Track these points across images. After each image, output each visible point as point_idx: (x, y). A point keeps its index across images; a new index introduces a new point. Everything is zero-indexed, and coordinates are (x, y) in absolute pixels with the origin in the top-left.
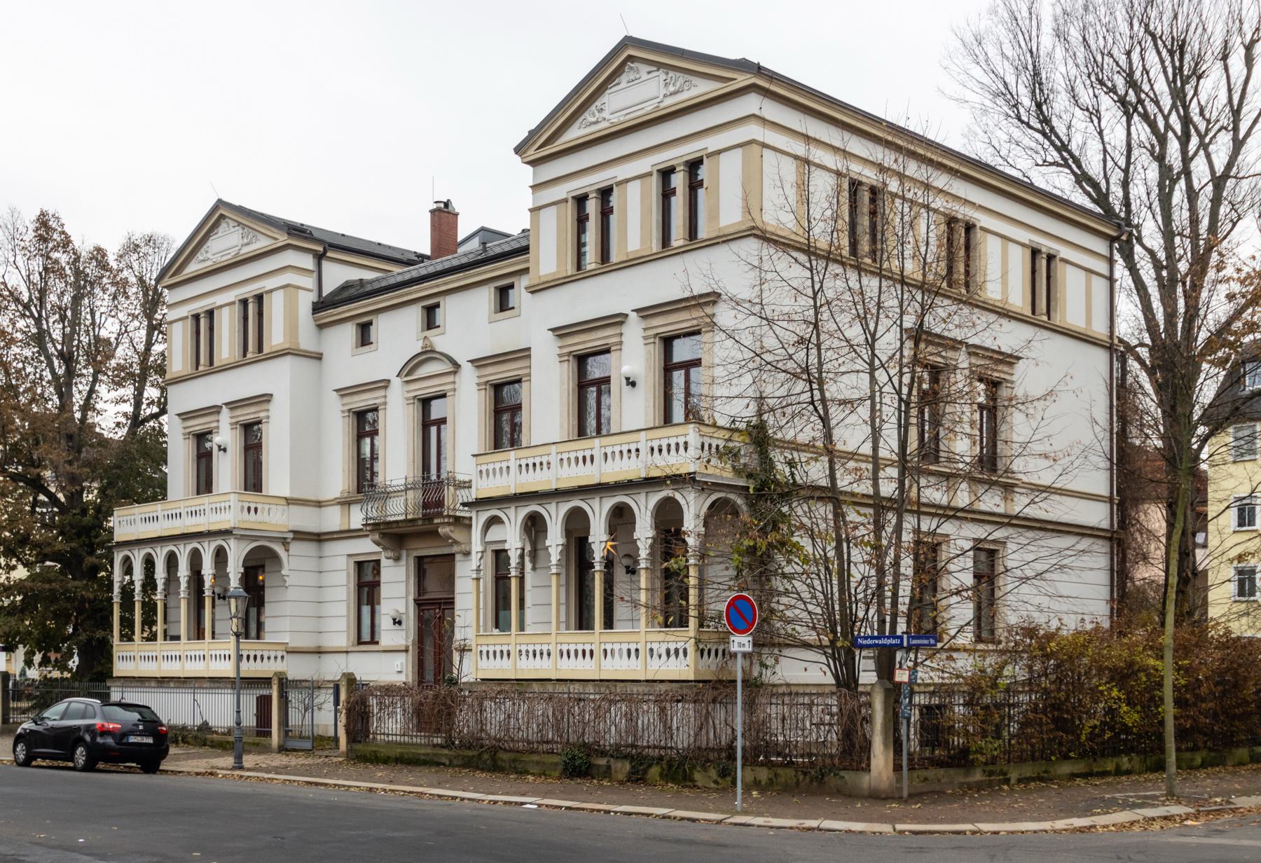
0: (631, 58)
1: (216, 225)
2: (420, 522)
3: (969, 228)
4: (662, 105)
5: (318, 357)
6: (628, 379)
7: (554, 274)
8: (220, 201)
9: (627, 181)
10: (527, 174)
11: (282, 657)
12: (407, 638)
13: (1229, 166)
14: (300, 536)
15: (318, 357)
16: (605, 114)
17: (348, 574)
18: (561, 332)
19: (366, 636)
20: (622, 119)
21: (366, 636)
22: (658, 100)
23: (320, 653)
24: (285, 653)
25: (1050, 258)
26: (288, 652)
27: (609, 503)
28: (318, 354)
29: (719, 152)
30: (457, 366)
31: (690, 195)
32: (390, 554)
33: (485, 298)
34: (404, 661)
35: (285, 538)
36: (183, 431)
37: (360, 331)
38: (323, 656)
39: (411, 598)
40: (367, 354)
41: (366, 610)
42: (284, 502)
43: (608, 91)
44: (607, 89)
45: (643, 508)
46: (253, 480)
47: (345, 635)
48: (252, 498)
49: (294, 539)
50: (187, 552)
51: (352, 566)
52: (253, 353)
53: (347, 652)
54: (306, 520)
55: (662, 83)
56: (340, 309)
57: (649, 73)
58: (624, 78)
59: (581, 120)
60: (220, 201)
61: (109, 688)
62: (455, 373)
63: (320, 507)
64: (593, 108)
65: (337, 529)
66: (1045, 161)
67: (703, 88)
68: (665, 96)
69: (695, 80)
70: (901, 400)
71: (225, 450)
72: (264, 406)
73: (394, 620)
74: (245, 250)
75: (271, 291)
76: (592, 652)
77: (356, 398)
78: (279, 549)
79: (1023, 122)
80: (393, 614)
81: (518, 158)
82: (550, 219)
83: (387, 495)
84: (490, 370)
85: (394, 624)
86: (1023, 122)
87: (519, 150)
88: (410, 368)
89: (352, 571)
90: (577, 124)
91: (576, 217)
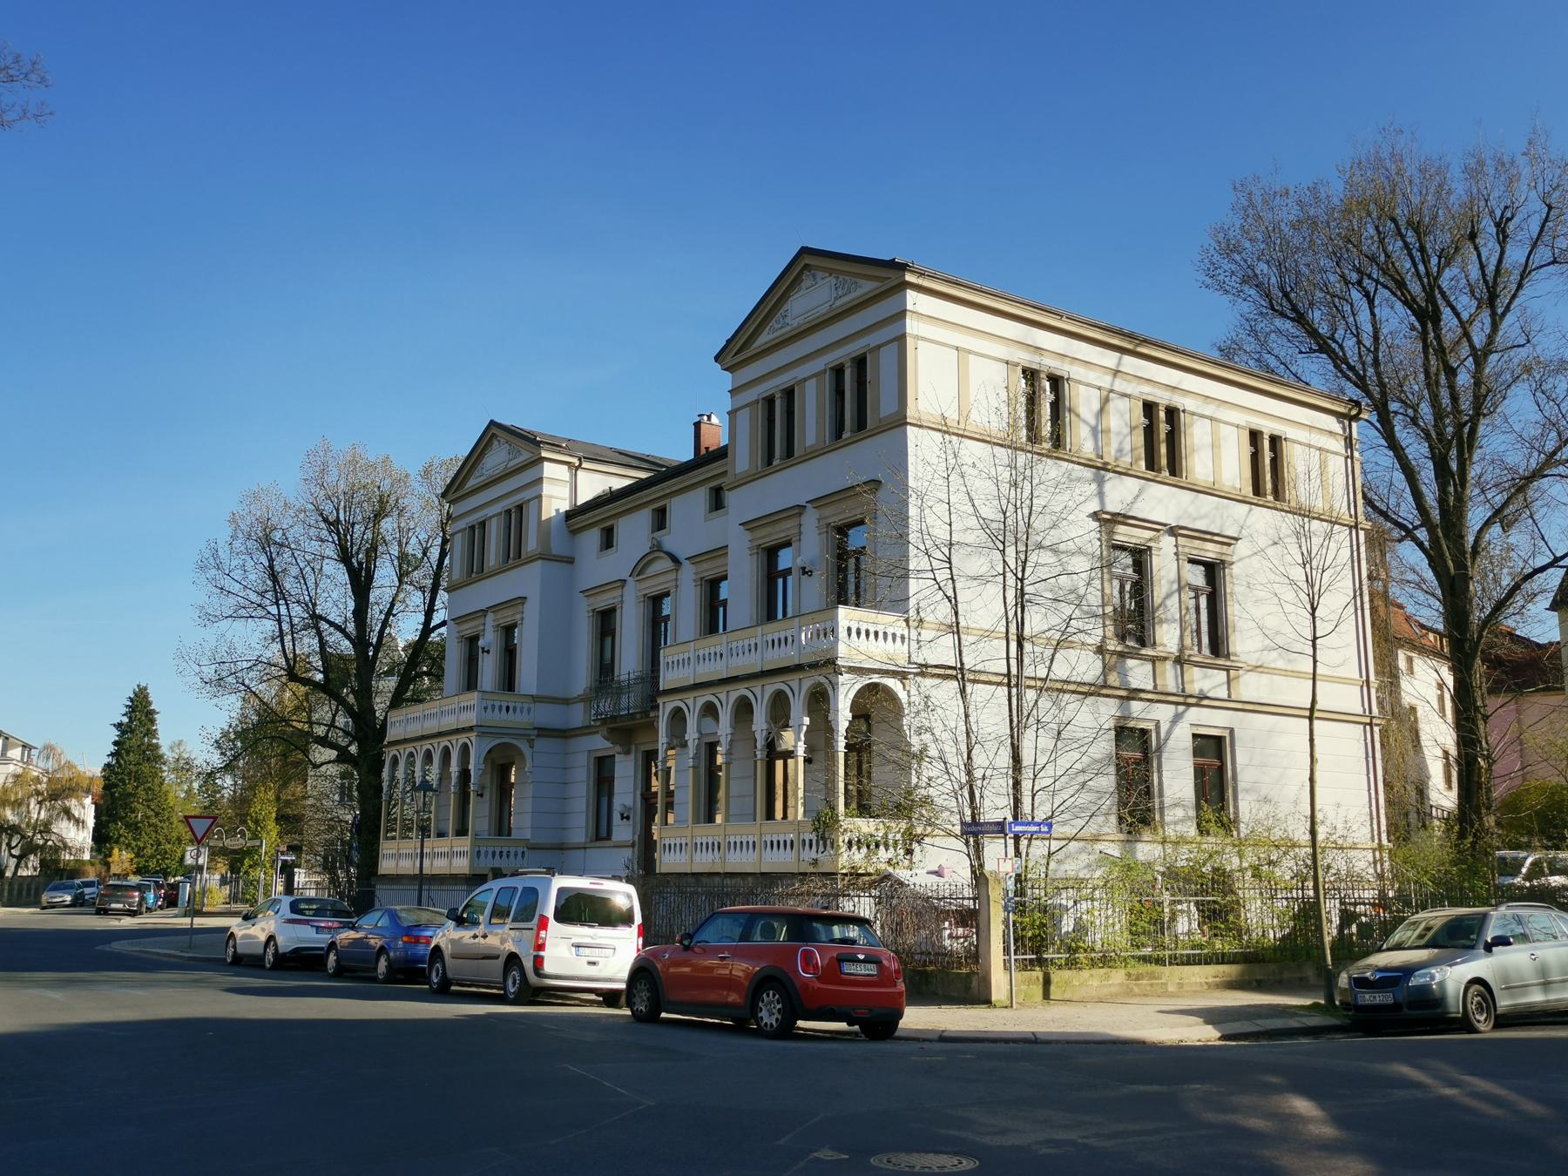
0: (806, 266)
1: (489, 443)
2: (638, 716)
3: (1172, 413)
8: (492, 423)
9: (805, 380)
11: (523, 853)
12: (634, 834)
13: (1491, 339)
14: (544, 732)
15: (570, 561)
16: (788, 320)
17: (588, 769)
21: (604, 833)
22: (830, 303)
23: (562, 849)
25: (1275, 440)
29: (879, 347)
31: (858, 389)
35: (529, 735)
36: (457, 635)
38: (565, 852)
39: (639, 793)
43: (791, 299)
46: (508, 680)
48: (507, 699)
49: (538, 736)
50: (732, 701)
53: (585, 848)
54: (545, 716)
55: (833, 289)
56: (588, 515)
60: (492, 423)
61: (374, 886)
62: (677, 570)
65: (581, 725)
66: (1310, 349)
68: (836, 299)
69: (861, 281)
70: (1017, 578)
71: (488, 652)
73: (622, 815)
74: (511, 464)
75: (529, 501)
77: (599, 598)
78: (523, 746)
79: (1276, 311)
81: (718, 366)
83: (620, 691)
84: (705, 566)
86: (1276, 311)
88: (640, 568)
89: (592, 767)
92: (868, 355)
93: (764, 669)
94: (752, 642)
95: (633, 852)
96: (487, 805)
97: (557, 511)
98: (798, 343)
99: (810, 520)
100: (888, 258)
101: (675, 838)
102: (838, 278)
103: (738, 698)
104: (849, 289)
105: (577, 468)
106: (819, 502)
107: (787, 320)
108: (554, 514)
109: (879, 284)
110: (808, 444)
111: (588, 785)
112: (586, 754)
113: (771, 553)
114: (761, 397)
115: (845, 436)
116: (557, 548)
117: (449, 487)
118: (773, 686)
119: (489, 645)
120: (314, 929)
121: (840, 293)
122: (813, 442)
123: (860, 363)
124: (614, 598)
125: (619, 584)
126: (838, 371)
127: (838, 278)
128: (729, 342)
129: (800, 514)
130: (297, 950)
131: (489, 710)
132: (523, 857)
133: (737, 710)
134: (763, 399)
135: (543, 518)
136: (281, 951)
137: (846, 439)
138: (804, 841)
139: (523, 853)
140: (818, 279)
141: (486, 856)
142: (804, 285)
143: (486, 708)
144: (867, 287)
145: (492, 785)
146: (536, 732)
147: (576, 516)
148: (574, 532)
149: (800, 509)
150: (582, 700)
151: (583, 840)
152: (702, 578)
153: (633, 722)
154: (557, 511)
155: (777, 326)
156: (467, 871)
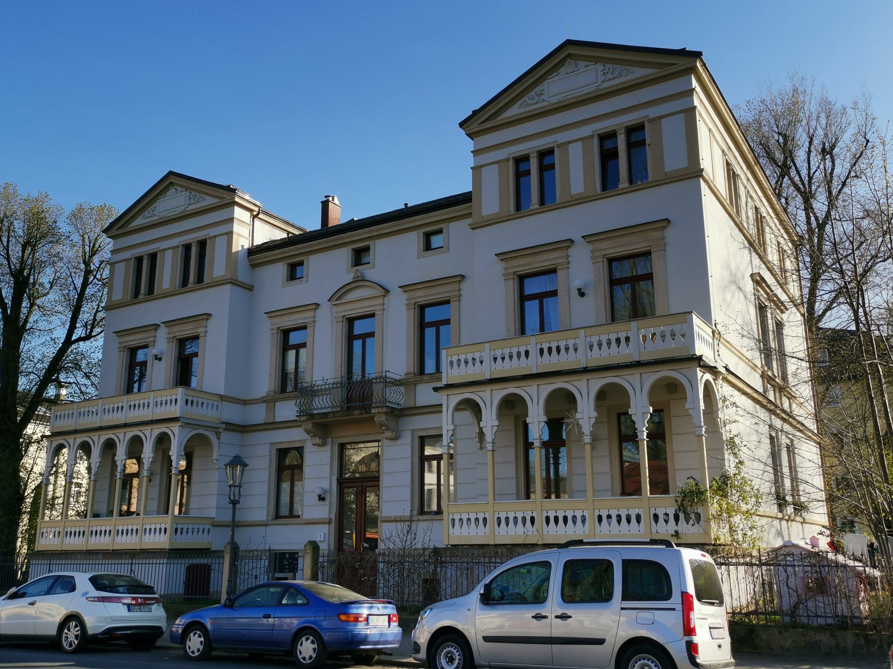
4: (188, 209)
5: (250, 288)
6: (579, 290)
7: (497, 214)
9: (165, 250)
10: (469, 144)
11: (209, 530)
12: (330, 512)
14: (231, 427)
15: (250, 288)
16: (545, 97)
18: (503, 256)
19: (285, 511)
20: (561, 99)
21: (285, 511)
22: (185, 207)
24: (211, 527)
26: (213, 526)
27: (547, 388)
28: (251, 286)
29: (216, 236)
30: (387, 291)
32: (317, 440)
33: (414, 239)
34: (326, 531)
35: (217, 428)
37: (290, 268)
40: (296, 285)
41: (286, 486)
42: (219, 399)
44: (546, 79)
45: (535, 400)
47: (265, 510)
49: (225, 429)
50: (154, 436)
51: (274, 452)
52: (194, 284)
53: (266, 525)
54: (231, 413)
55: (188, 198)
57: (586, 66)
58: (563, 71)
59: (521, 102)
62: (384, 296)
63: (245, 405)
64: (533, 93)
65: (262, 422)
67: (640, 73)
71: (160, 359)
72: (204, 323)
73: (319, 496)
76: (485, 520)
77: (285, 319)
78: (212, 436)
80: (319, 491)
82: (491, 176)
85: (319, 500)
87: (461, 125)
88: (338, 296)
90: (517, 105)
91: (198, 253)
92: (208, 240)
93: (492, 377)
94: (146, 401)
95: (329, 528)
96: (157, 489)
97: (243, 246)
98: (578, 109)
99: (162, 334)
100: (225, 184)
101: (101, 526)
102: (191, 193)
103: (82, 442)
104: (198, 200)
105: (254, 217)
106: (169, 323)
107: (155, 213)
108: (240, 248)
109: (219, 200)
110: (164, 288)
111: (270, 471)
112: (268, 446)
113: (133, 351)
114: (181, 244)
115: (140, 297)
116: (243, 275)
117: (112, 225)
118: (158, 430)
119: (162, 353)
120: (126, 607)
121: (192, 201)
122: (223, 273)
123: (202, 244)
124: (308, 318)
125: (459, 279)
126: (187, 247)
127: (191, 193)
128: (475, 113)
129: (156, 330)
130: (110, 631)
131: (596, 347)
132: (208, 533)
133: (131, 442)
134: (598, 135)
135: (234, 250)
136: (90, 631)
137: (623, 189)
138: (118, 530)
139: (209, 530)
140: (178, 192)
141: (516, 523)
142: (168, 193)
143: (495, 359)
144: (209, 201)
145: (162, 472)
146: (224, 426)
147: (253, 251)
148: (254, 266)
149: (156, 326)
150: (264, 401)
151: (264, 518)
152: (416, 303)
153: (327, 420)
154: (243, 246)
155: (148, 215)
156: (167, 547)
